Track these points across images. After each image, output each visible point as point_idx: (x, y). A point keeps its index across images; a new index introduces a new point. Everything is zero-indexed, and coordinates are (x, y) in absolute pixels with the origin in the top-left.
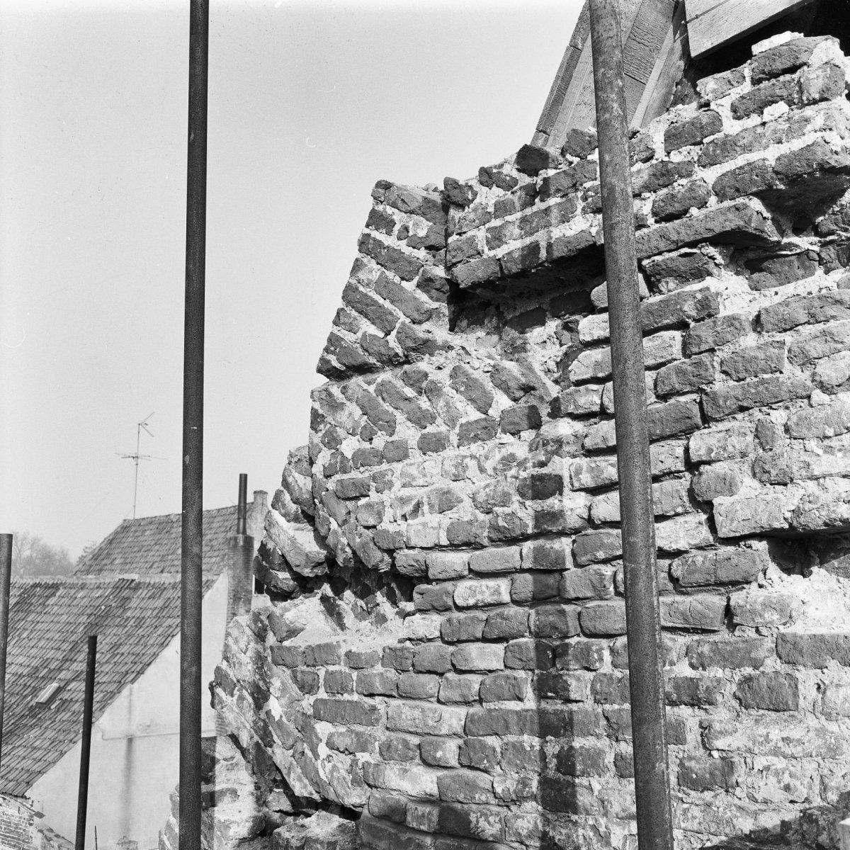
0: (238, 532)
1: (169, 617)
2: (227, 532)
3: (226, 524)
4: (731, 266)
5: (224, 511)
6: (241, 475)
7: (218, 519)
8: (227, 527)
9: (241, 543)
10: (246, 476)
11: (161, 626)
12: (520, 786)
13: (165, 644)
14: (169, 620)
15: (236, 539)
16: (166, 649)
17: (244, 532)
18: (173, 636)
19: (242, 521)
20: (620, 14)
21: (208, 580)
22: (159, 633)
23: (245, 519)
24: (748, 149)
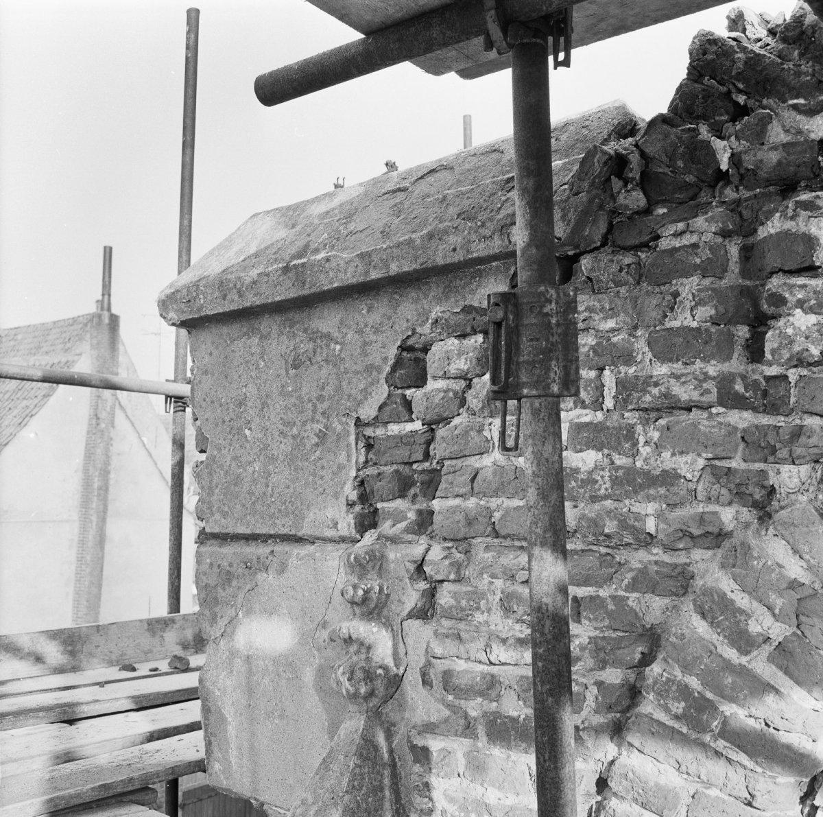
0: (102, 309)
1: (24, 399)
2: (66, 343)
3: (64, 335)
4: (600, 736)
5: (62, 323)
6: (105, 248)
7: (54, 331)
8: (65, 338)
9: (106, 321)
10: (111, 249)
11: (16, 407)
12: (369, 390)
13: (22, 425)
14: (25, 402)
15: (100, 316)
16: (24, 429)
17: (109, 309)
18: (32, 416)
19: (106, 297)
20: (604, 808)
21: (68, 362)
22: (14, 414)
23: (109, 295)
24: (752, 591)
